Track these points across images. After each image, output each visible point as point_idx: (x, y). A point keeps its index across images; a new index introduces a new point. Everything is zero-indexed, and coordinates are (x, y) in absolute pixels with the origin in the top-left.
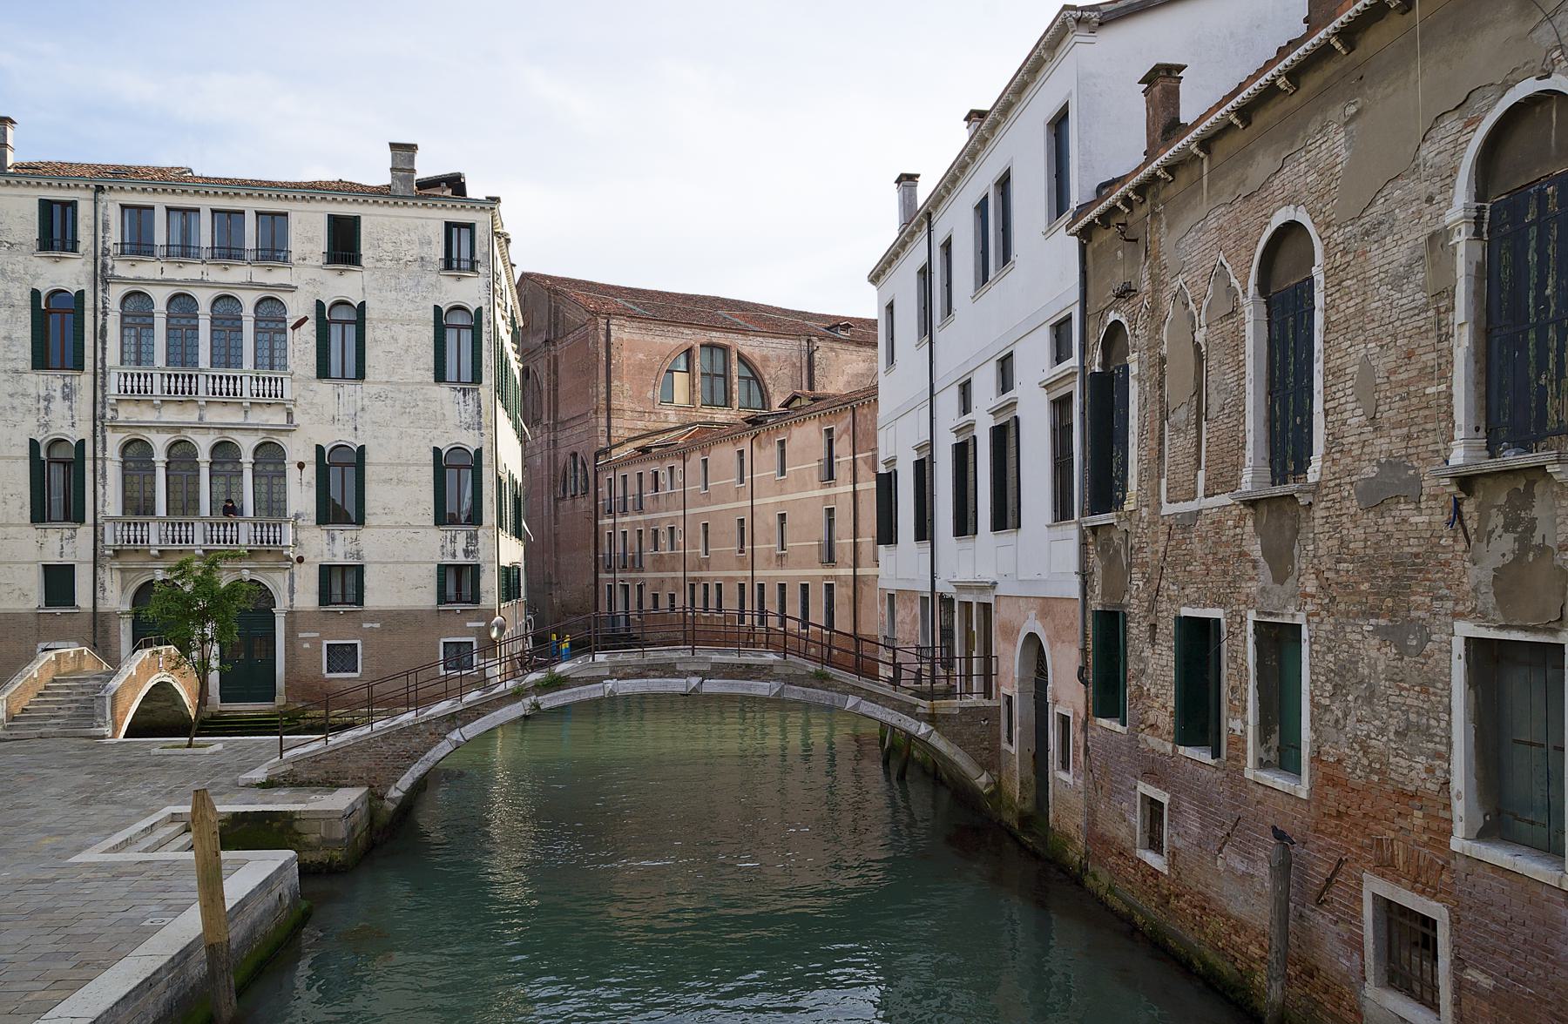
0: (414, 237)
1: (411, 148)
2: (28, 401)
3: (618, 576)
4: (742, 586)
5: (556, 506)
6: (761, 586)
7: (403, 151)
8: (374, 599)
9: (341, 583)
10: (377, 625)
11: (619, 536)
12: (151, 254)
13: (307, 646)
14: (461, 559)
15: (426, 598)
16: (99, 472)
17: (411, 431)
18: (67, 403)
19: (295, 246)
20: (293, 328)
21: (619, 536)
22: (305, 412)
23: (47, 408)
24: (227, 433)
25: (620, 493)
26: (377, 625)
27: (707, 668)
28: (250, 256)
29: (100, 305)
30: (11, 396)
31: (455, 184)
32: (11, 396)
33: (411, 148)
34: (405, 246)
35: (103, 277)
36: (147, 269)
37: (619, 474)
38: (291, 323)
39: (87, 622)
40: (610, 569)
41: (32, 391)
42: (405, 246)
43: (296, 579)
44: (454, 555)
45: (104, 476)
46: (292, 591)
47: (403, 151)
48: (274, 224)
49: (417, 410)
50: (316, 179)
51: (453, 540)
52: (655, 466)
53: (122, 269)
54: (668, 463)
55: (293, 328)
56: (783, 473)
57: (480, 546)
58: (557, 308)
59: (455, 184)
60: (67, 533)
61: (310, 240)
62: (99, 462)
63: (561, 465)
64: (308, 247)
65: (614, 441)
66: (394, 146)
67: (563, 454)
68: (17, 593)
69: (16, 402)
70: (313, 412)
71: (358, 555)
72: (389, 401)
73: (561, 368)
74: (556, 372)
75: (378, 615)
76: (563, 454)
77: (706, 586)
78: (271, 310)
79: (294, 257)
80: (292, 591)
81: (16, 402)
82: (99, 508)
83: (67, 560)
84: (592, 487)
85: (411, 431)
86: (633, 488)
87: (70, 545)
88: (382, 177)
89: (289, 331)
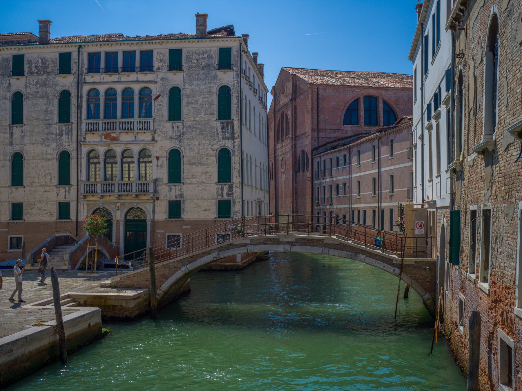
0: (206, 56)
1: (205, 16)
2: (53, 136)
3: (322, 207)
4: (374, 211)
5: (296, 176)
6: (383, 211)
7: (201, 19)
8: (186, 216)
9: (175, 209)
10: (189, 227)
11: (322, 188)
12: (134, 71)
13: (159, 236)
14: (226, 197)
15: (212, 214)
16: (79, 164)
17: (204, 142)
18: (67, 136)
19: (156, 64)
20: (155, 100)
21: (322, 188)
22: (159, 136)
23: (60, 139)
24: (128, 146)
25: (322, 168)
26: (189, 227)
27: (293, 240)
28: (137, 69)
29: (80, 95)
30: (47, 134)
31: (229, 31)
32: (47, 134)
33: (205, 16)
34: (202, 61)
35: (80, 83)
36: (97, 78)
37: (323, 158)
38: (153, 97)
39: (74, 225)
40: (318, 205)
41: (54, 132)
42: (202, 61)
43: (156, 207)
44: (222, 195)
45: (81, 164)
46: (154, 212)
47: (201, 19)
48: (147, 56)
49: (206, 132)
50: (170, 33)
51: (222, 189)
52: (337, 155)
53: (89, 78)
54: (343, 153)
55: (155, 100)
56: (392, 155)
57: (234, 191)
58: (296, 83)
59: (229, 31)
60: (67, 189)
61: (161, 61)
62: (79, 160)
63: (298, 156)
64: (161, 64)
65: (321, 143)
66: (198, 16)
67: (299, 152)
68: (49, 214)
69: (49, 137)
70: (163, 135)
71: (181, 196)
72: (194, 129)
73: (298, 111)
74: (295, 113)
75: (189, 223)
76: (299, 152)
77: (359, 212)
78: (145, 93)
79: (155, 69)
80: (154, 212)
81: (49, 137)
82: (79, 179)
83: (67, 200)
84: (310, 166)
85: (204, 142)
86: (328, 165)
87: (69, 194)
88: (193, 31)
89: (153, 101)
